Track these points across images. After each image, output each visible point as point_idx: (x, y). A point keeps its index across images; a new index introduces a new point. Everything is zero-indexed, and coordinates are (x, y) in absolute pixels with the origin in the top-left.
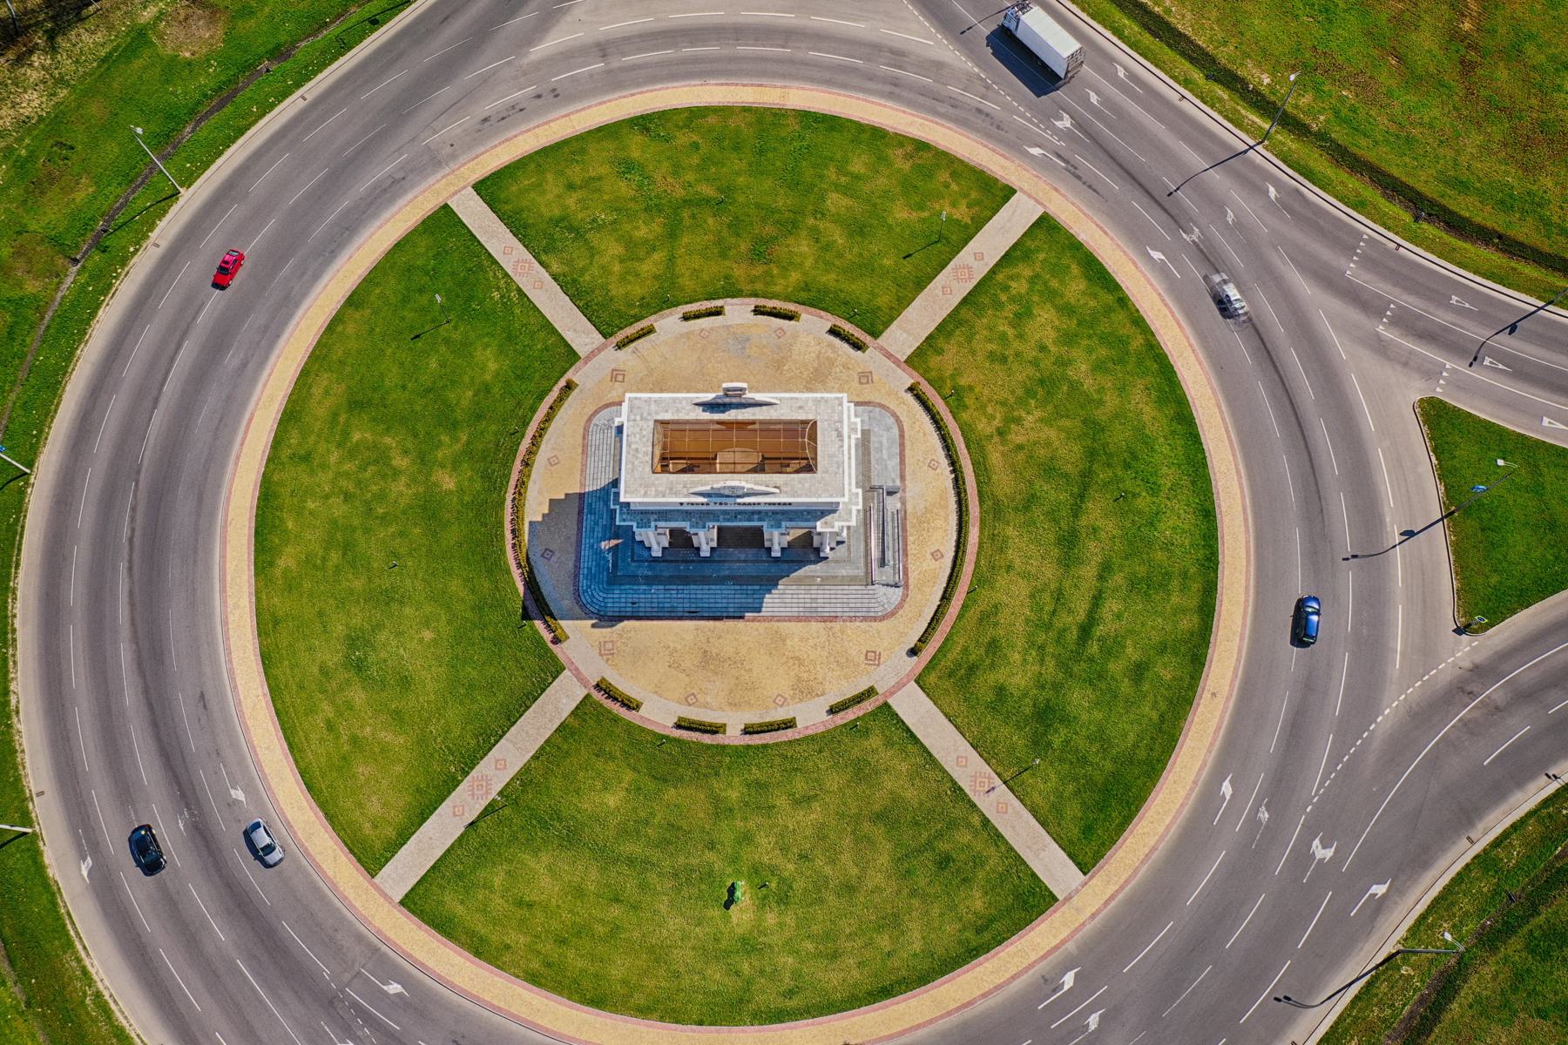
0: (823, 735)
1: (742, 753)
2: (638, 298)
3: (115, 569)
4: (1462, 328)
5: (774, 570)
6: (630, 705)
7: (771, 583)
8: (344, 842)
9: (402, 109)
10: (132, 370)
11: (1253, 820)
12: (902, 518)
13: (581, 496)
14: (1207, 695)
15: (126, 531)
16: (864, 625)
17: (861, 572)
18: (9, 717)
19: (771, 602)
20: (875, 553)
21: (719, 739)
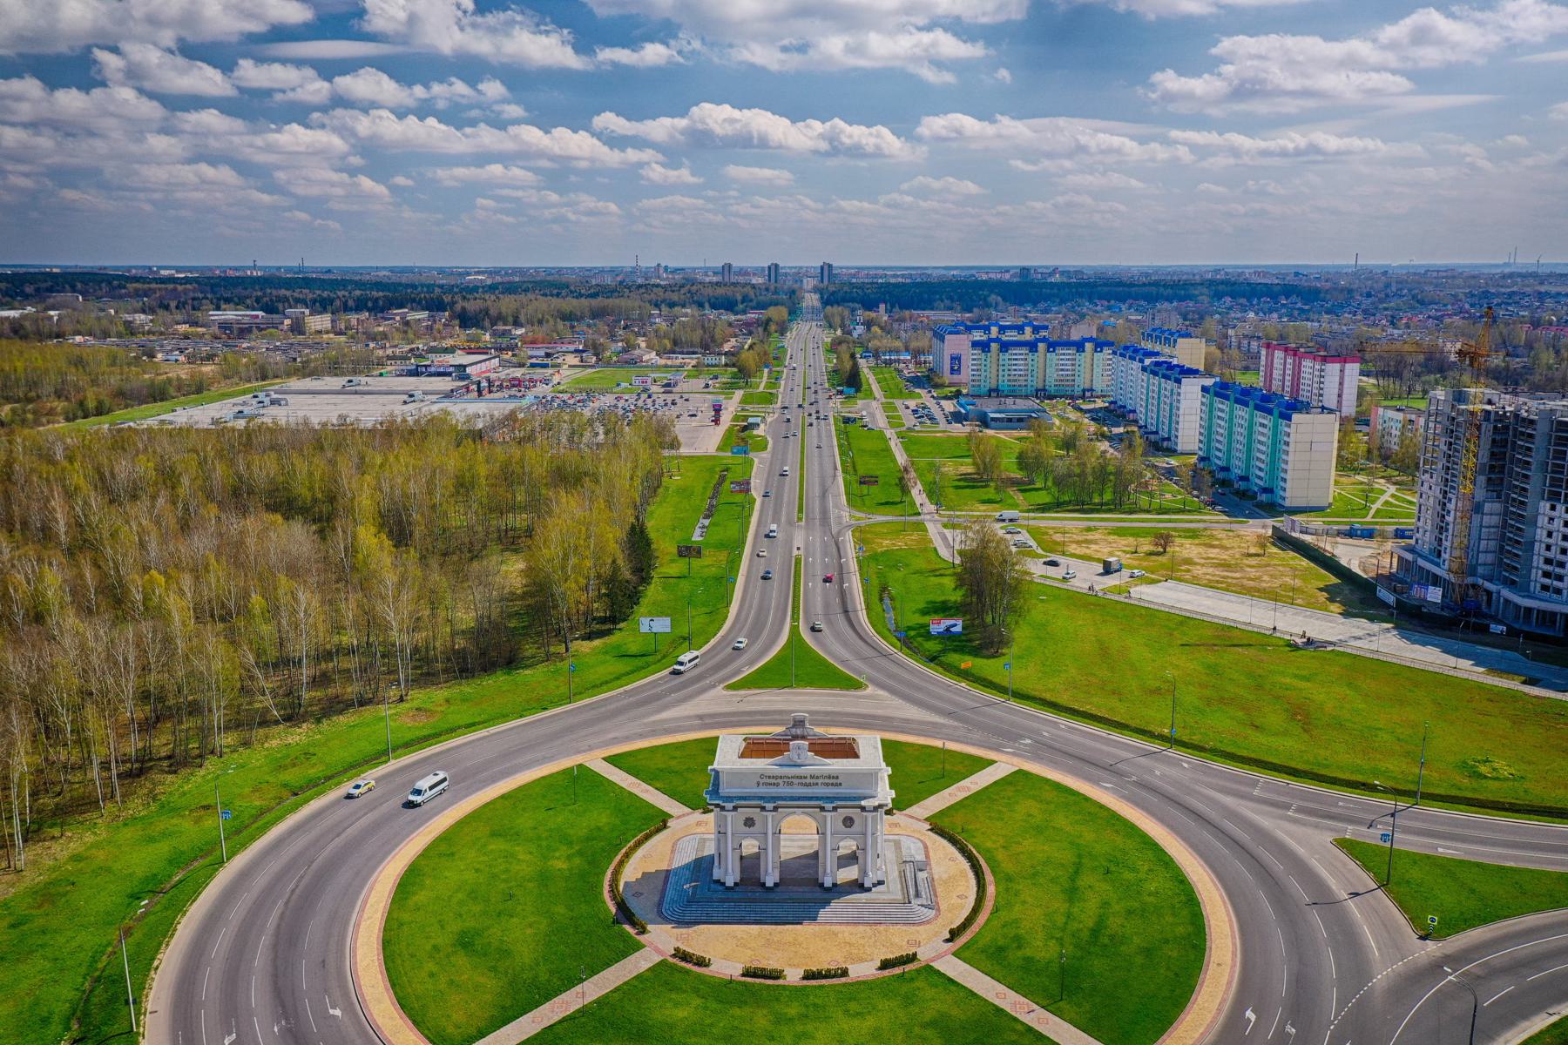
0: (873, 981)
1: (796, 992)
2: (1122, 345)
3: (275, 903)
4: (821, 694)
5: (826, 896)
6: (702, 962)
7: (827, 903)
8: (428, 1038)
9: (571, 729)
10: (895, 669)
11: (1281, 1031)
12: (931, 882)
13: (668, 871)
14: (1212, 966)
15: (292, 886)
16: (904, 928)
17: (899, 896)
18: (149, 970)
19: (823, 914)
20: (912, 892)
21: (781, 982)
